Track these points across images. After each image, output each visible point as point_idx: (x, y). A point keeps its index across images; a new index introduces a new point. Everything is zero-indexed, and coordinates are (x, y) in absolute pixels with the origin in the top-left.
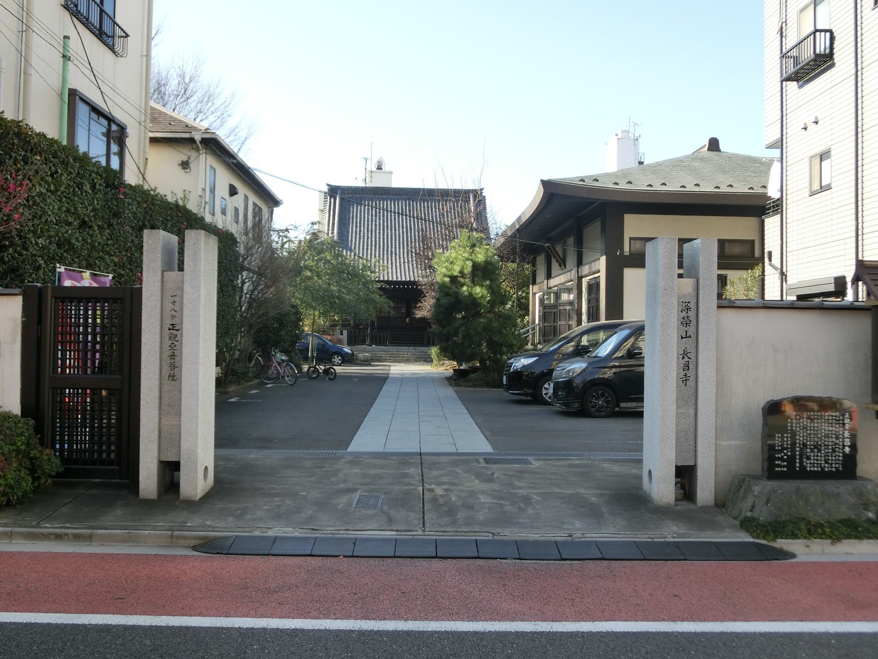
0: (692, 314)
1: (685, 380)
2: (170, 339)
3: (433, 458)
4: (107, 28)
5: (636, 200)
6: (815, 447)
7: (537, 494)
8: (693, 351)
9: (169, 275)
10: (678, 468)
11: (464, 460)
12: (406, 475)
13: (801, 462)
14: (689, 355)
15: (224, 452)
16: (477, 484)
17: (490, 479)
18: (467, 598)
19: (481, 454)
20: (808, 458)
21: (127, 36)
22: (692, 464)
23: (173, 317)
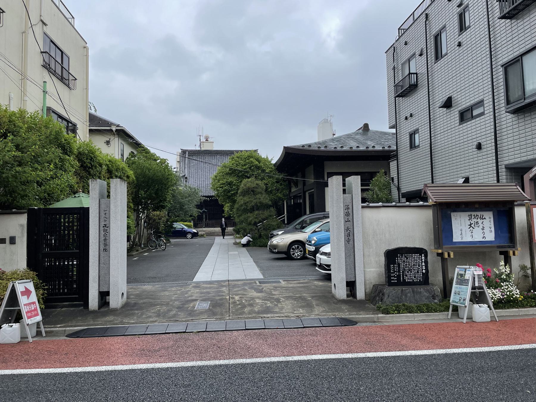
0: (350, 211)
1: (348, 241)
2: (104, 231)
3: (236, 282)
4: (65, 75)
5: (330, 154)
6: (409, 270)
7: (283, 297)
8: (352, 227)
9: (103, 201)
10: (347, 282)
11: (250, 283)
12: (220, 291)
13: (403, 278)
15: (134, 285)
16: (255, 294)
17: (261, 291)
18: (249, 348)
19: (257, 279)
20: (406, 276)
21: (76, 79)
22: (354, 280)
23: (105, 221)
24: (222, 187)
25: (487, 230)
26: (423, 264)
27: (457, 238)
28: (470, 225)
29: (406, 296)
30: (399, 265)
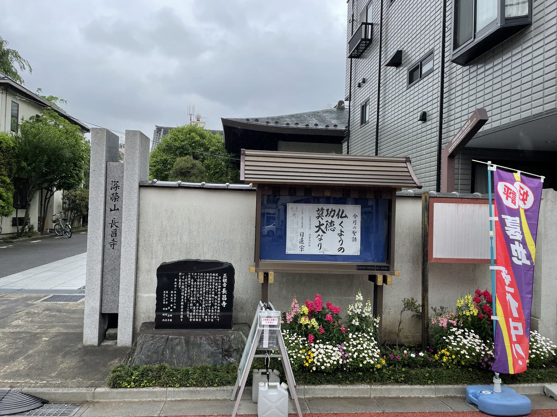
14: (117, 224)
24: (155, 166)
25: (348, 237)
26: (224, 291)
27: (292, 247)
28: (319, 227)
29: (172, 351)
30: (179, 291)
